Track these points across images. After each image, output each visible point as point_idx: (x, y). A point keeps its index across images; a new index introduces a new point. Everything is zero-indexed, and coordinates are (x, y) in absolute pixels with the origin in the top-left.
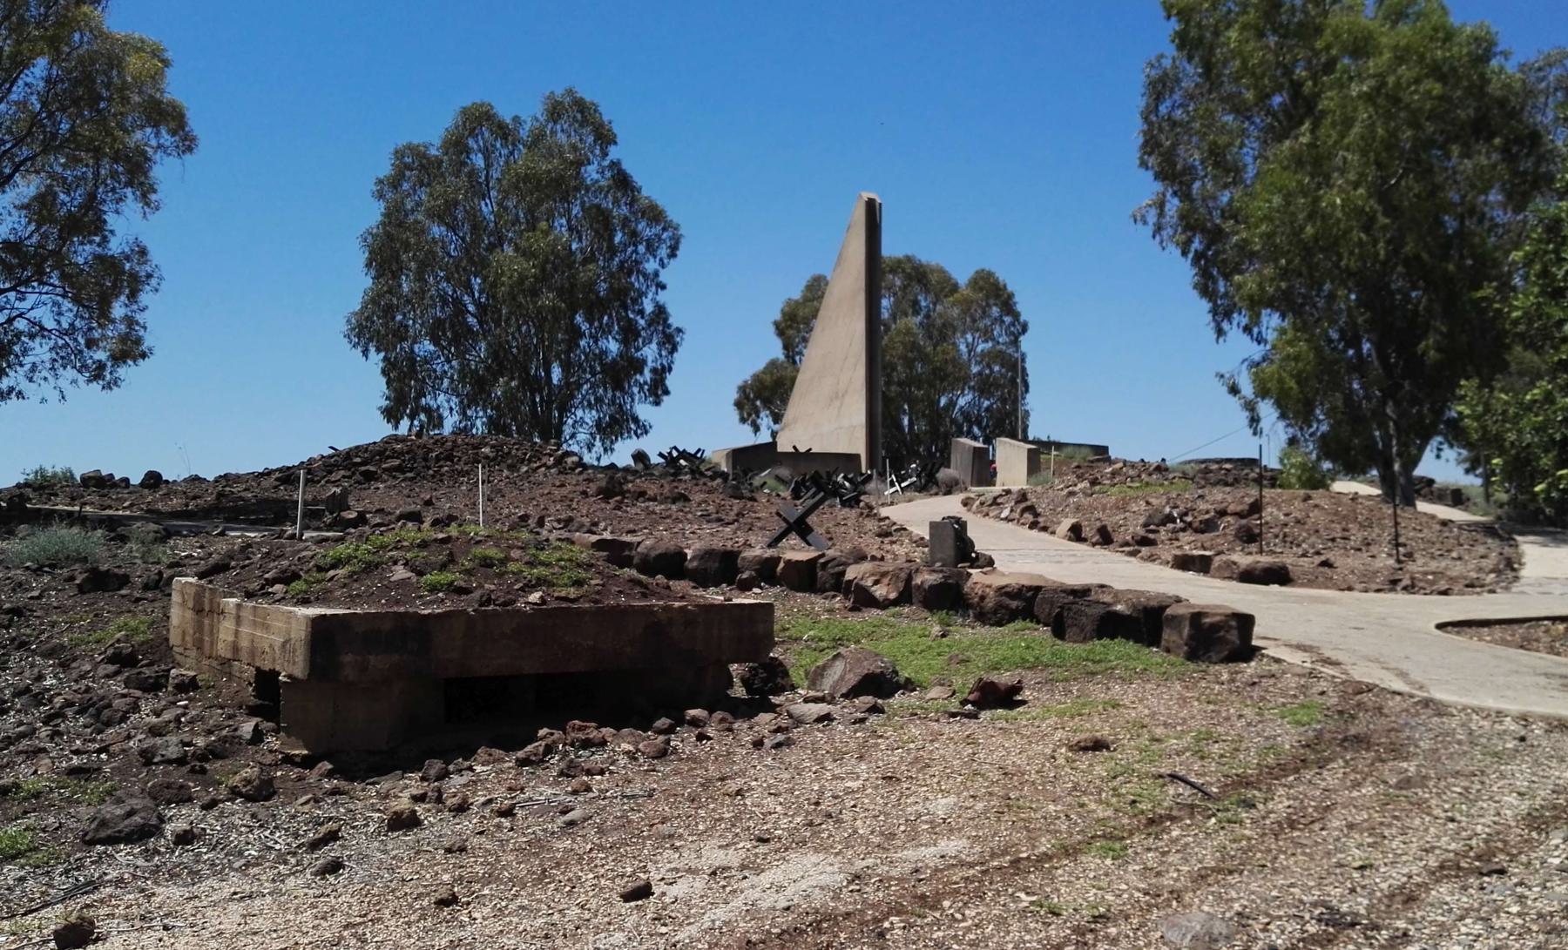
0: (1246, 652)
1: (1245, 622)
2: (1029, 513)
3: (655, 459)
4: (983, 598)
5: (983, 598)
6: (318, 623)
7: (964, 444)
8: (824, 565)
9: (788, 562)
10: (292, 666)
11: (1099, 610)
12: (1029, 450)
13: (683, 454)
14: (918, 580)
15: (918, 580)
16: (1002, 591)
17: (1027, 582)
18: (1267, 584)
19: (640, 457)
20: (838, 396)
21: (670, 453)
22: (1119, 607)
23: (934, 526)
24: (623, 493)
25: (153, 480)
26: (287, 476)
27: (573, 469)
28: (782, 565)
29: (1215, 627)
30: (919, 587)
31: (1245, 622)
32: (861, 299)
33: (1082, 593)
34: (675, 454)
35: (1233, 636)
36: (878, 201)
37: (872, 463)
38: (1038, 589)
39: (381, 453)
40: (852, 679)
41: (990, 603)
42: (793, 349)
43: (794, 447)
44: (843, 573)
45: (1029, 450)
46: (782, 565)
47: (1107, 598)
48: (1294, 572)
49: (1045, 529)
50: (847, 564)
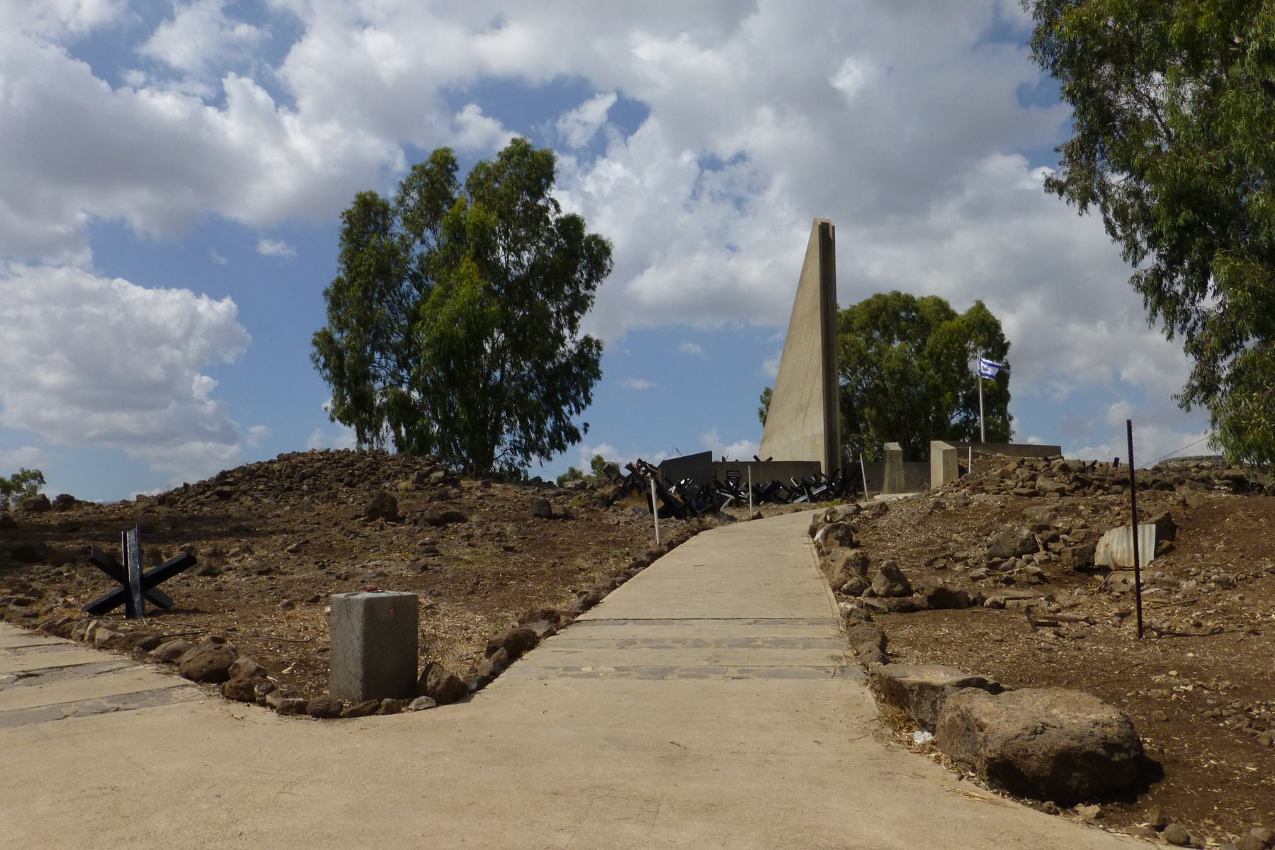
12: (945, 452)
20: (803, 408)
36: (831, 225)
43: (755, 457)
45: (945, 452)
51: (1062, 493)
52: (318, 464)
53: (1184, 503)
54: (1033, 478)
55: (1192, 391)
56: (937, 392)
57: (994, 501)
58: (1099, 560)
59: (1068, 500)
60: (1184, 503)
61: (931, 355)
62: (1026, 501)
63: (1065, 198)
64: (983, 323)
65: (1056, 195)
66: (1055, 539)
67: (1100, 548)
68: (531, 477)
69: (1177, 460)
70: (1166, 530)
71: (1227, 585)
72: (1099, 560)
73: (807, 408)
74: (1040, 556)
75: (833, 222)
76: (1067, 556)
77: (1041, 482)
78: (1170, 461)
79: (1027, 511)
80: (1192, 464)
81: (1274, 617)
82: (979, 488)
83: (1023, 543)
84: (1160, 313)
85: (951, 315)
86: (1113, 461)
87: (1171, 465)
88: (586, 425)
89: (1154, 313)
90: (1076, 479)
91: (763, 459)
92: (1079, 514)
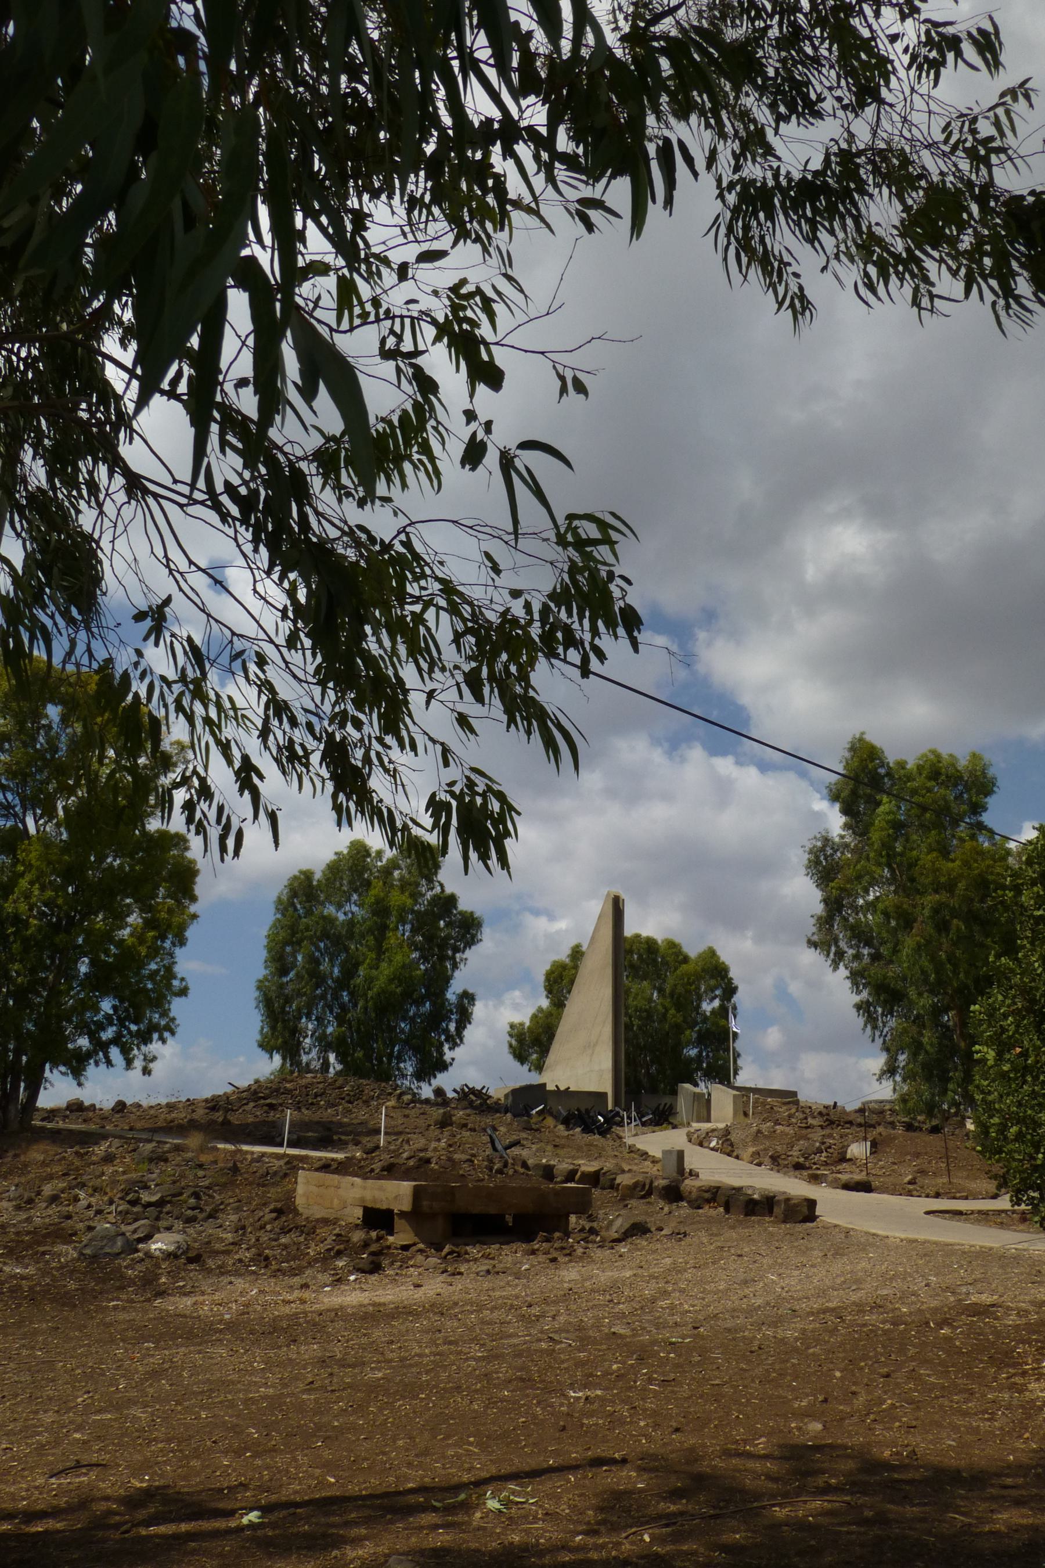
0: (811, 1217)
1: (812, 1204)
2: (728, 1147)
3: (451, 1095)
4: (690, 1193)
5: (690, 1193)
6: (415, 1186)
7: (687, 1089)
8: (604, 1174)
9: (583, 1173)
10: (406, 1206)
11: (746, 1198)
13: (473, 1091)
14: (656, 1184)
15: (656, 1184)
16: (700, 1189)
17: (713, 1184)
18: (858, 1191)
19: (439, 1092)
21: (463, 1090)
22: (756, 1196)
23: (665, 1152)
24: (451, 1125)
25: (138, 1106)
26: (214, 1104)
27: (408, 1104)
28: (579, 1174)
29: (796, 1205)
30: (657, 1187)
31: (812, 1204)
32: (609, 972)
33: (739, 1189)
34: (466, 1090)
35: (805, 1210)
37: (617, 1102)
38: (718, 1188)
39: (277, 1090)
40: (627, 1226)
41: (694, 1196)
42: (559, 1003)
44: (615, 1179)
45: (735, 1096)
46: (579, 1174)
47: (750, 1192)
48: (875, 1183)
49: (737, 1157)
50: (616, 1174)
51: (822, 1127)
52: (321, 1086)
53: (880, 1134)
54: (806, 1118)
55: (883, 1073)
56: (678, 1029)
57: (790, 1130)
58: (848, 1156)
59: (827, 1131)
60: (880, 1134)
61: (672, 994)
62: (804, 1132)
63: (818, 951)
64: (716, 968)
65: (813, 949)
66: (830, 1147)
67: (849, 1151)
68: (423, 1097)
69: (876, 1102)
70: (874, 1144)
71: (894, 1163)
72: (848, 1156)
73: (595, 1046)
74: (824, 1154)
75: (623, 896)
76: (835, 1155)
77: (810, 1121)
78: (871, 1102)
79: (810, 1136)
80: (888, 1107)
81: (1041, 1391)
82: (777, 1123)
83: (817, 1149)
84: (869, 1027)
85: (686, 959)
86: (832, 1104)
87: (871, 1105)
88: (453, 1059)
89: (865, 1026)
90: (827, 1120)
91: (562, 1088)
92: (834, 1139)
